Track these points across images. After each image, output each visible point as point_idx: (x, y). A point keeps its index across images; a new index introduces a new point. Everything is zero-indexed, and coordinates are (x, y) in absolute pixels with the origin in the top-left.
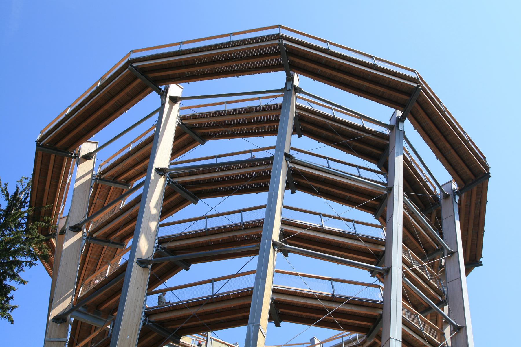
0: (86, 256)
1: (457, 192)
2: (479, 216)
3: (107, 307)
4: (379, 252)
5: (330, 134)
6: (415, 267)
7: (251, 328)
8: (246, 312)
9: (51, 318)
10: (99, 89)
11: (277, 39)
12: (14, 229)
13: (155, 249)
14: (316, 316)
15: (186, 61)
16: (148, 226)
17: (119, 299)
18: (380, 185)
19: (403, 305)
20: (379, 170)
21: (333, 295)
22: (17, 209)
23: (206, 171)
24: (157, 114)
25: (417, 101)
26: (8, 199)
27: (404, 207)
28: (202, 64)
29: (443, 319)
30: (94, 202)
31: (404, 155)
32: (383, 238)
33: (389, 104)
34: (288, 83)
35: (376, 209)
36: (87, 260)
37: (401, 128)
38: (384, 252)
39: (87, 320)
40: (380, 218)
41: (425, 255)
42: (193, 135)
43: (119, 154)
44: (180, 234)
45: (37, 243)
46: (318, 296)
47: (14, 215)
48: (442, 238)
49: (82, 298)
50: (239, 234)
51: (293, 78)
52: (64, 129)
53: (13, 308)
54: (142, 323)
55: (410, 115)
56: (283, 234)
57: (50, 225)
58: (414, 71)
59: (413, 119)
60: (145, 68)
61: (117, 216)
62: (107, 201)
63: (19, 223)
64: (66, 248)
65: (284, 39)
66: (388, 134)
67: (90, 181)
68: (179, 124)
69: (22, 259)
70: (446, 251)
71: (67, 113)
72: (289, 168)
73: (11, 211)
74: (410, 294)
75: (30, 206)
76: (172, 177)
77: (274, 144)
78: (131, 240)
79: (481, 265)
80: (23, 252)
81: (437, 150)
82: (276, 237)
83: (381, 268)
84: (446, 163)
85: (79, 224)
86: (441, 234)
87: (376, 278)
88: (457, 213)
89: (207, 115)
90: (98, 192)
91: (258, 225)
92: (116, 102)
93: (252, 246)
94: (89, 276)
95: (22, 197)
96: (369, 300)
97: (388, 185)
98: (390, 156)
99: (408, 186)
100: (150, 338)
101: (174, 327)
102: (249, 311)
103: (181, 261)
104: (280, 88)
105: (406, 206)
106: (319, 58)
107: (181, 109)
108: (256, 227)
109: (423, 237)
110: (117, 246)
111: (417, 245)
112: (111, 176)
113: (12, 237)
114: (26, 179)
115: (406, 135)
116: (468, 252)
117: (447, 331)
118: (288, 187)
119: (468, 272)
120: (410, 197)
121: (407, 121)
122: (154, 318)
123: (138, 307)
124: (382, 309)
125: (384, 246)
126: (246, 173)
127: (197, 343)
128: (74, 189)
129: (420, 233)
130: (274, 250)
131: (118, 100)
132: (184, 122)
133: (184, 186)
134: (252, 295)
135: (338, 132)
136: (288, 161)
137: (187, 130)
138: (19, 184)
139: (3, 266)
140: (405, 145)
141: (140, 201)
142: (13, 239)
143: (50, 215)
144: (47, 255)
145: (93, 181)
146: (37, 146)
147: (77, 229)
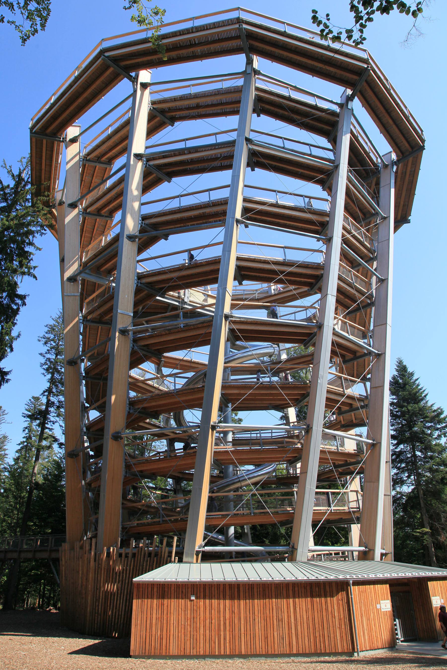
0: (84, 227)
1: (395, 162)
4: (324, 222)
9: (65, 278)
11: (237, 23)
13: (140, 226)
16: (132, 206)
21: (285, 260)
24: (131, 99)
25: (366, 81)
26: (14, 179)
30: (84, 179)
32: (328, 209)
33: (340, 84)
34: (248, 66)
35: (324, 182)
36: (84, 230)
37: (349, 107)
39: (92, 279)
40: (327, 189)
48: (378, 206)
50: (207, 210)
51: (252, 61)
52: (51, 117)
53: (35, 267)
55: (358, 94)
59: (361, 97)
60: (116, 57)
61: (105, 194)
64: (68, 223)
65: (244, 23)
68: (150, 109)
69: (34, 229)
72: (249, 150)
76: (148, 160)
79: (409, 222)
81: (381, 126)
82: (238, 215)
83: (324, 238)
84: (388, 137)
85: (75, 202)
88: (393, 181)
89: (175, 99)
90: (85, 171)
91: (224, 202)
92: (93, 90)
95: (23, 175)
96: (314, 263)
97: (336, 163)
102: (218, 274)
104: (241, 71)
105: (349, 179)
106: (276, 41)
107: (151, 93)
108: (222, 204)
110: (107, 219)
112: (95, 157)
114: (24, 158)
118: (248, 165)
122: (144, 281)
124: (323, 269)
125: (329, 216)
128: (67, 171)
130: (237, 225)
131: (95, 88)
132: (155, 106)
133: (159, 167)
137: (158, 114)
140: (353, 120)
143: (49, 190)
144: (52, 224)
146: (30, 133)
147: (74, 206)
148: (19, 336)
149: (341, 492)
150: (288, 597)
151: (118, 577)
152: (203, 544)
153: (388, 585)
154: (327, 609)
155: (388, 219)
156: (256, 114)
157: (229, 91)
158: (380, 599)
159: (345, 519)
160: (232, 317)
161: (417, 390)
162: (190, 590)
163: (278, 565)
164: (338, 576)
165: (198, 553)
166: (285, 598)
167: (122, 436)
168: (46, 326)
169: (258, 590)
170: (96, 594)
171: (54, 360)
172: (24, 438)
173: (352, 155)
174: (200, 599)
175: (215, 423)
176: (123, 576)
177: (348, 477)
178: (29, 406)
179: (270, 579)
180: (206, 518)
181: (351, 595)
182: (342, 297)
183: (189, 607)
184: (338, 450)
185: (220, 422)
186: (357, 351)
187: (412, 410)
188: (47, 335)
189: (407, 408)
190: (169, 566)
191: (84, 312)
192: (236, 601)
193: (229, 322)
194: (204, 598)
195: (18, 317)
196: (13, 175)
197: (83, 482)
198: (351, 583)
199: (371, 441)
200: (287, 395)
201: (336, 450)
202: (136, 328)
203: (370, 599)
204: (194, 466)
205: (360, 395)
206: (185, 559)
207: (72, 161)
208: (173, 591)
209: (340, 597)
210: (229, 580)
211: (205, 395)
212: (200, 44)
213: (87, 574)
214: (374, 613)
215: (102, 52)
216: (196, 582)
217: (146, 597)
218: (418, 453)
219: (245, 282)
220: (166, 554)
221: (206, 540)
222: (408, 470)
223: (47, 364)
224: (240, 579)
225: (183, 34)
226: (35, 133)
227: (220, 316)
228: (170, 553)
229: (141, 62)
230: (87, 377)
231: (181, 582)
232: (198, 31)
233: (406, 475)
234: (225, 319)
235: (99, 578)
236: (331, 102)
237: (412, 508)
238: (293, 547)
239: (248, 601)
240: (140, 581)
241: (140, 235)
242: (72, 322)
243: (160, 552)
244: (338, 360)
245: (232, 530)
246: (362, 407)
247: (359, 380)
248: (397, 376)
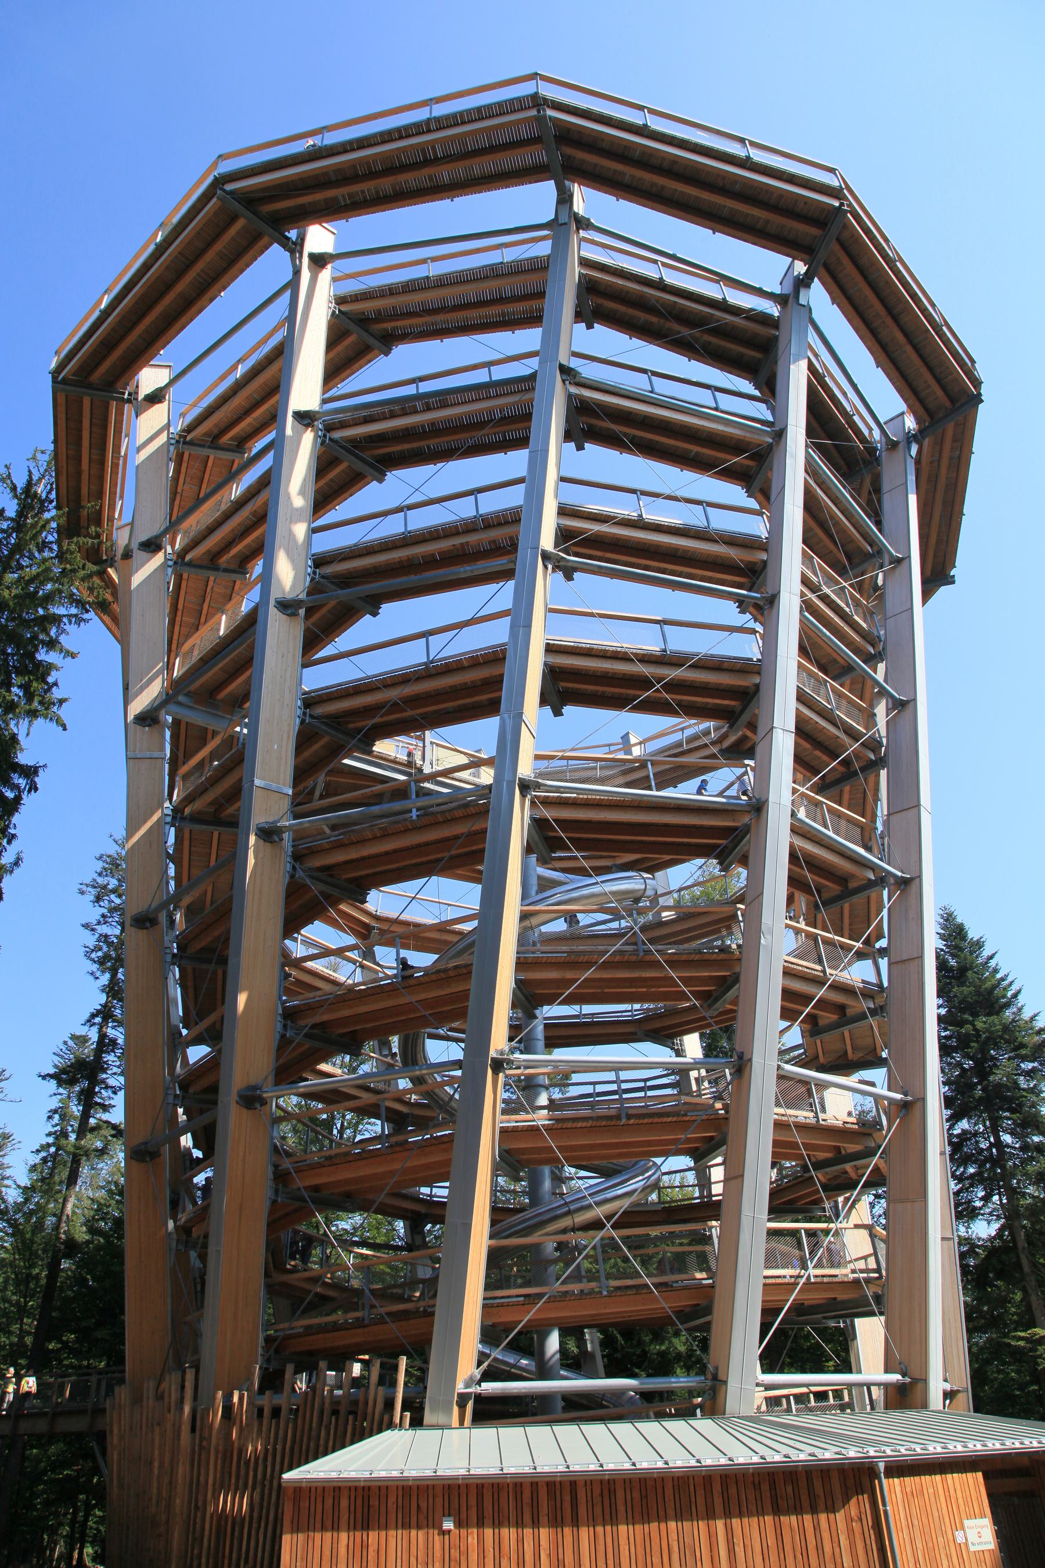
1: (914, 436)
2: (956, 484)
3: (230, 694)
4: (755, 563)
5: (654, 319)
6: (826, 590)
7: (507, 721)
8: (493, 692)
9: (131, 718)
10: (161, 249)
11: (534, 107)
12: (37, 554)
13: (308, 579)
14: (632, 692)
15: (338, 170)
17: (250, 677)
18: (759, 426)
19: (800, 666)
20: (757, 393)
21: (665, 651)
22: (36, 515)
23: (399, 413)
25: (839, 240)
26: (16, 496)
27: (806, 471)
28: (372, 174)
29: (874, 688)
30: (179, 490)
31: (810, 361)
32: (764, 534)
35: (751, 477)
36: (180, 607)
37: (802, 301)
38: (765, 563)
39: (197, 718)
41: (845, 567)
42: (365, 335)
43: (216, 386)
44: (355, 545)
45: (83, 580)
46: (635, 654)
47: (34, 526)
48: (880, 531)
49: (182, 678)
50: (472, 538)
51: (571, 196)
53: (61, 702)
54: (298, 721)
55: (822, 271)
56: (562, 535)
57: (100, 543)
58: (832, 171)
59: (829, 279)
60: (252, 192)
61: (227, 516)
62: (204, 486)
63: (44, 542)
64: (138, 586)
65: (548, 106)
66: (776, 314)
67: (165, 449)
68: (334, 312)
69: (61, 611)
70: (886, 558)
71: (103, 306)
72: (570, 397)
73: (25, 520)
74: (814, 645)
75: (58, 508)
76: (329, 428)
77: (536, 346)
78: (261, 563)
79: (953, 582)
80: (61, 598)
82: (547, 541)
83: (758, 595)
86: (878, 523)
87: (748, 616)
88: (911, 478)
89: (391, 291)
90: (183, 470)
91: (511, 519)
92: (198, 275)
93: (499, 563)
94: (188, 637)
95: (40, 489)
96: (735, 658)
97: (776, 424)
98: (780, 363)
99: (815, 425)
100: (316, 747)
101: (360, 724)
102: (501, 690)
103: (361, 598)
104: (544, 221)
105: (811, 469)
106: (625, 147)
107: (335, 280)
108: (507, 523)
109: (842, 531)
110: (234, 576)
111: (832, 547)
112: (206, 434)
113: (35, 570)
114: (43, 452)
115: (814, 316)
116: (931, 553)
117: (881, 710)
118: (568, 436)
119: (926, 595)
120: (819, 448)
121: (816, 283)
122: (320, 710)
123: (287, 691)
124: (759, 673)
125: (766, 550)
126: (482, 410)
127: (406, 751)
128: (137, 467)
129: (837, 523)
130: (546, 567)
131: (202, 270)
132: (344, 308)
133: (356, 445)
134: (504, 658)
135: (670, 314)
136: (567, 382)
137: (352, 327)
138: (32, 464)
139: (30, 627)
140: (812, 338)
141: (269, 483)
142: (38, 575)
143: (99, 523)
144: (105, 600)
145: (172, 448)
146: (53, 382)
147: (153, 547)
148: (17, 863)
149: (831, 1230)
150: (710, 1515)
151: (251, 1473)
152: (477, 1374)
153: (980, 1475)
154: (820, 1548)
155: (906, 562)
156: (584, 324)
157: (517, 269)
158: (963, 1515)
159: (843, 1302)
160: (538, 786)
161: (994, 982)
162: (439, 1501)
163: (677, 1426)
164: (843, 1451)
165: (463, 1400)
166: (702, 1519)
167: (265, 1095)
168: (100, 858)
169: (629, 1497)
170: (195, 1523)
171: (117, 937)
172: (49, 1135)
174: (467, 1526)
175: (502, 1053)
176: (265, 1468)
177: (841, 1199)
178: (62, 1057)
179: (660, 1464)
180: (485, 1306)
181: (884, 1505)
182: (807, 745)
183: (438, 1553)
184: (818, 1121)
185: (512, 1051)
186: (853, 876)
187: (987, 1030)
188: (100, 880)
189: (974, 1026)
190: (388, 1436)
191: (175, 797)
192: (567, 1530)
193: (533, 803)
194: (480, 1524)
195: (16, 819)
196: (14, 488)
197: (171, 1224)
198: (882, 1470)
199: (899, 1096)
200: (686, 981)
201: (813, 1121)
202: (300, 823)
203: (936, 1514)
204: (448, 1173)
205: (863, 982)
206: (428, 1418)
207: (151, 445)
208: (392, 1507)
209: (854, 1512)
210: (547, 1469)
211: (473, 985)
212: (449, 158)
213: (172, 1470)
214: (949, 1557)
215: (219, 182)
216: (455, 1478)
217: (318, 1525)
218: (1007, 1138)
220: (380, 1406)
221: (486, 1364)
222: (982, 1181)
223: (100, 949)
224: (577, 1468)
225: (408, 136)
226: (64, 381)
227: (508, 782)
228: (389, 1404)
229: (310, 203)
230: (181, 958)
231: (415, 1479)
232: (441, 129)
233: (981, 1194)
234: (521, 792)
235: (202, 1479)
236: (759, 292)
237: (1000, 1275)
238: (715, 1377)
239: (600, 1529)
240: (300, 1481)
241: (310, 598)
242: (145, 821)
243: (362, 1399)
244: (802, 901)
245: (553, 1343)
246: (873, 1012)
247: (858, 945)
248: (942, 950)
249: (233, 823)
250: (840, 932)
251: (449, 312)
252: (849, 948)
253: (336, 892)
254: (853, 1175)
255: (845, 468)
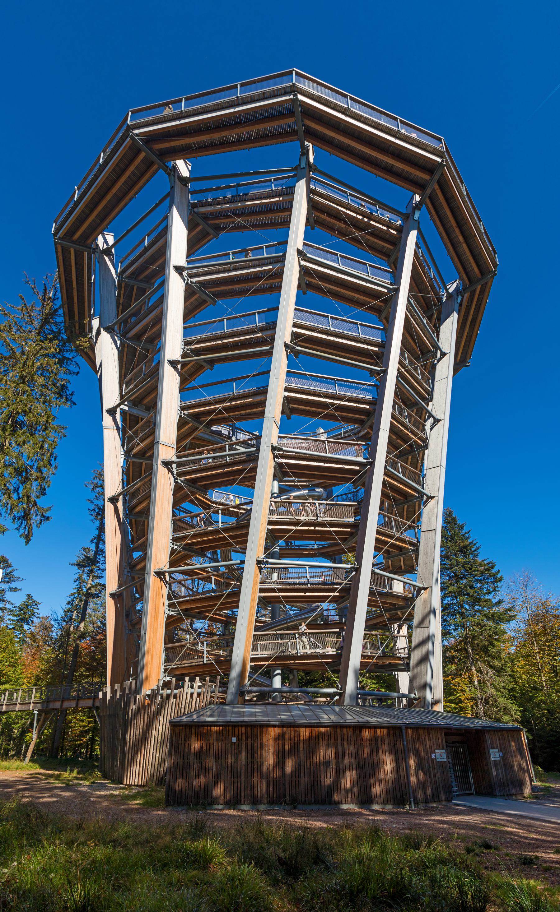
6: (410, 367)
13: (182, 350)
25: (439, 182)
90: (122, 292)
120: (416, 298)
137: (200, 221)
160: (281, 449)
173: (413, 282)
219: (293, 416)
249: (151, 458)
250: (402, 517)
251: (246, 216)
252: (404, 524)
253: (195, 490)
254: (400, 615)
255: (426, 308)
